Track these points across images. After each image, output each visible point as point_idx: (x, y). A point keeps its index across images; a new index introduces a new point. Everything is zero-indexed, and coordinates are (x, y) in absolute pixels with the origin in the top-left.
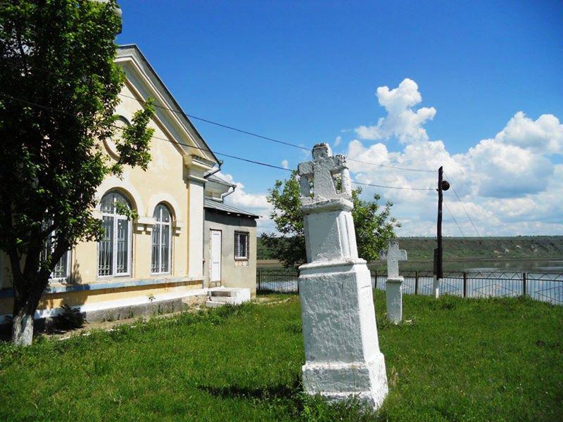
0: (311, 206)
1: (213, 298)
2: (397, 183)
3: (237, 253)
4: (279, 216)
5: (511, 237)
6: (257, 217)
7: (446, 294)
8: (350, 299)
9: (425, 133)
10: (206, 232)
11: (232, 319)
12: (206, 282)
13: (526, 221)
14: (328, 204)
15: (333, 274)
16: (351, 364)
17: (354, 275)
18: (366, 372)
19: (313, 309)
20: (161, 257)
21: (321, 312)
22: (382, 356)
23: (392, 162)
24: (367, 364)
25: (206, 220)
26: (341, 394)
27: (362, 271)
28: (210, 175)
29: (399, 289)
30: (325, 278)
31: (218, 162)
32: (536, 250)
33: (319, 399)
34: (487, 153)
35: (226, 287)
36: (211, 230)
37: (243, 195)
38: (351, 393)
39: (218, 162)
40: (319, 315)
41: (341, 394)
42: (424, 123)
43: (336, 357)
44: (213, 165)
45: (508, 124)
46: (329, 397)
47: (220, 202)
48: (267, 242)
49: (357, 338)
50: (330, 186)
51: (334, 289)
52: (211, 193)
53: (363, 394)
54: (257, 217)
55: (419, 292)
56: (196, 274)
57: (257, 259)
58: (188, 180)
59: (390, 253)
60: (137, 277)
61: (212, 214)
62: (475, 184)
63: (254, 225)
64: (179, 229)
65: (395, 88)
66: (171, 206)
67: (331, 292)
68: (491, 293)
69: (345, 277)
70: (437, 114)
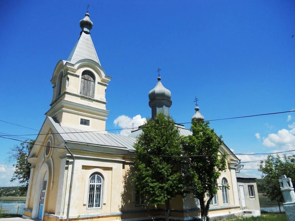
1: (245, 214)
4: (265, 176)
12: (241, 207)
20: (226, 198)
31: (239, 160)
35: (248, 209)
36: (239, 186)
39: (239, 160)
40: (290, 215)
48: (261, 189)
51: (292, 209)
56: (237, 204)
61: (239, 180)
66: (226, 179)
67: (292, 209)
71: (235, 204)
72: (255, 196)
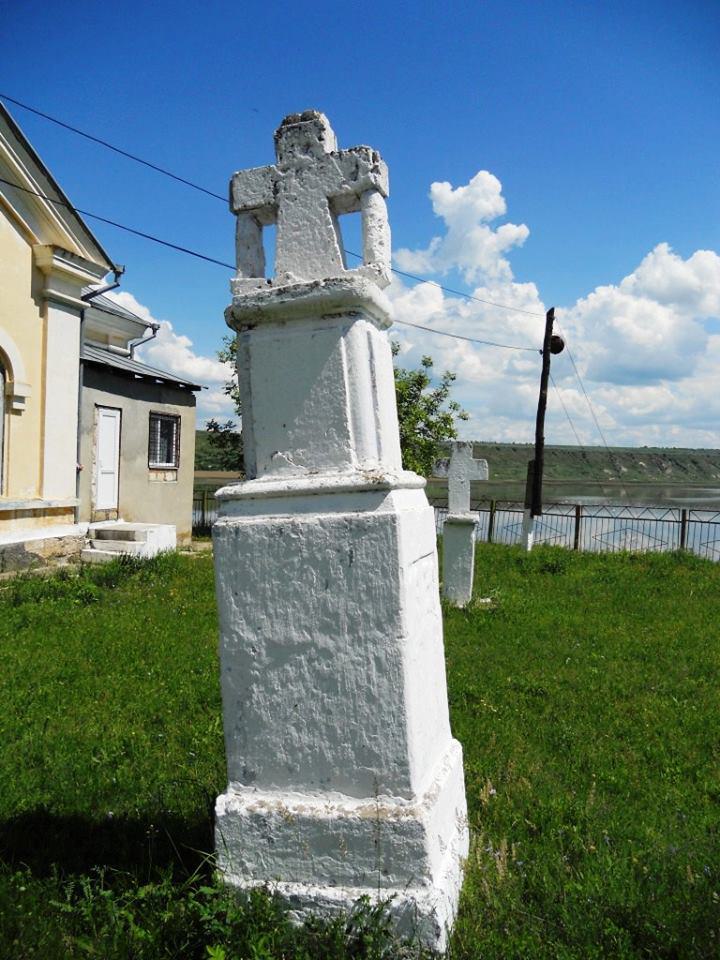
0: (260, 298)
1: (97, 543)
2: (456, 350)
3: (155, 454)
5: (632, 449)
6: (198, 388)
7: (546, 545)
8: (372, 598)
9: (509, 269)
10: (84, 410)
11: (127, 591)
12: (83, 511)
13: (658, 423)
14: (316, 293)
15: (323, 516)
16: (369, 803)
17: (389, 525)
18: (416, 830)
19: (257, 628)
21: (279, 637)
22: (456, 749)
23: (449, 316)
24: (418, 803)
25: (84, 385)
26: (332, 893)
27: (411, 510)
28: (95, 294)
29: (470, 538)
30: (295, 527)
31: (113, 268)
32: (669, 471)
33: (264, 912)
34: (606, 309)
36: (97, 406)
37: (190, 357)
38: (364, 891)
40: (272, 646)
41: (332, 893)
42: (507, 251)
43: (322, 779)
44: (102, 273)
45: (643, 263)
46: (295, 898)
47: (126, 356)
48: (217, 438)
49: (396, 725)
50: (326, 245)
52: (107, 336)
53: (399, 897)
54: (198, 388)
55: (496, 538)
56: (60, 493)
57: (195, 469)
58: (43, 300)
59: (454, 465)
60: (10, 497)
62: (582, 360)
63: (191, 402)
64: (21, 399)
65: (462, 186)
67: (314, 575)
68: (623, 543)
69: (360, 529)
70: (530, 236)
71: (45, 491)
72: (177, 465)
